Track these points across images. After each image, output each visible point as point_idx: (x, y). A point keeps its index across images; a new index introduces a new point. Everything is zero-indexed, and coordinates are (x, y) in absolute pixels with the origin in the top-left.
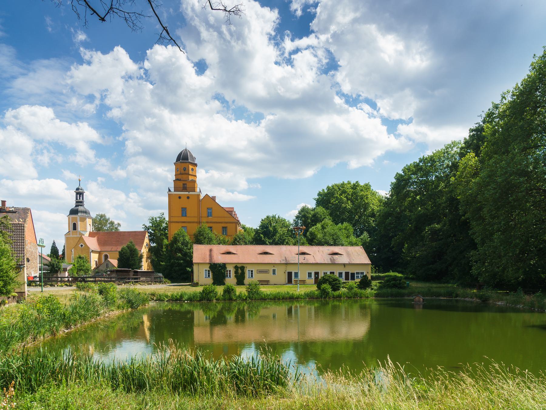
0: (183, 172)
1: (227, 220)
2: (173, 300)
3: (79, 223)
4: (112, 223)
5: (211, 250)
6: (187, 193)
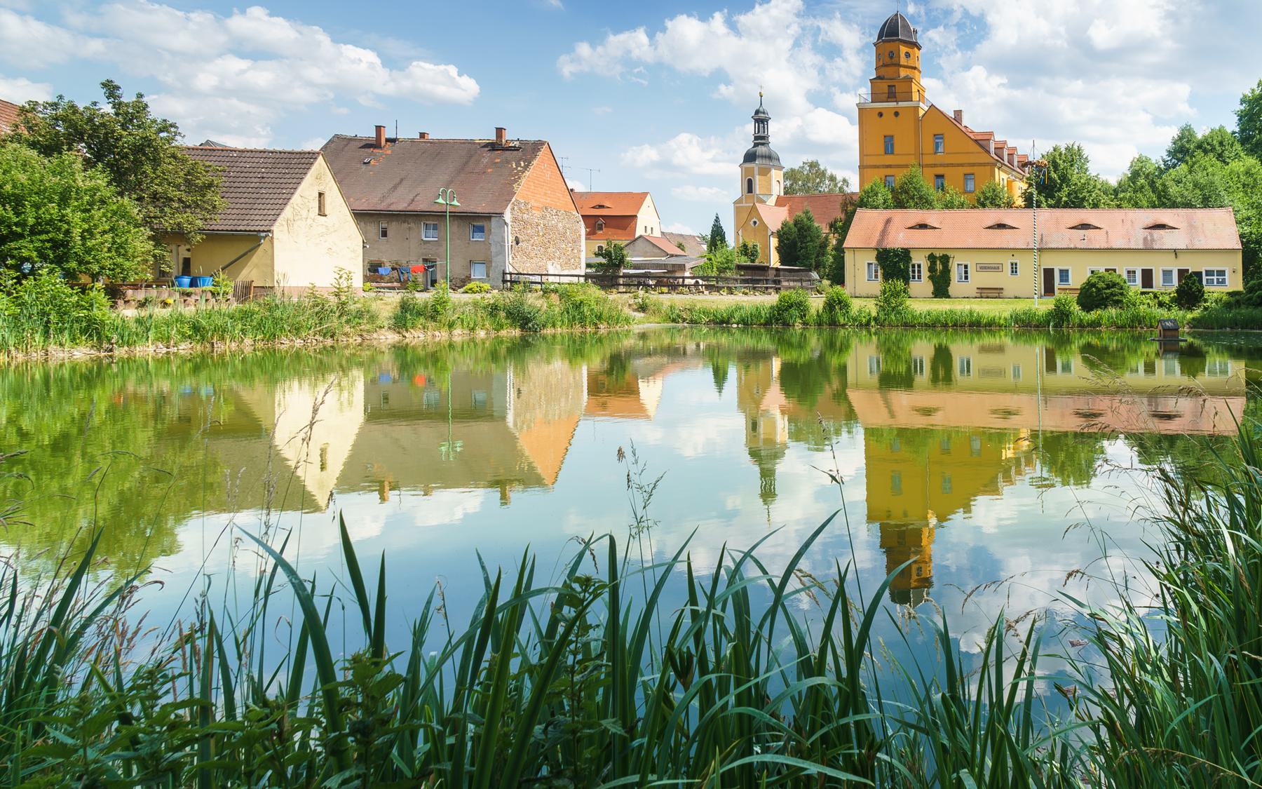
0: (887, 60)
2: (716, 323)
3: (757, 177)
4: (832, 179)
5: (888, 221)
6: (893, 104)
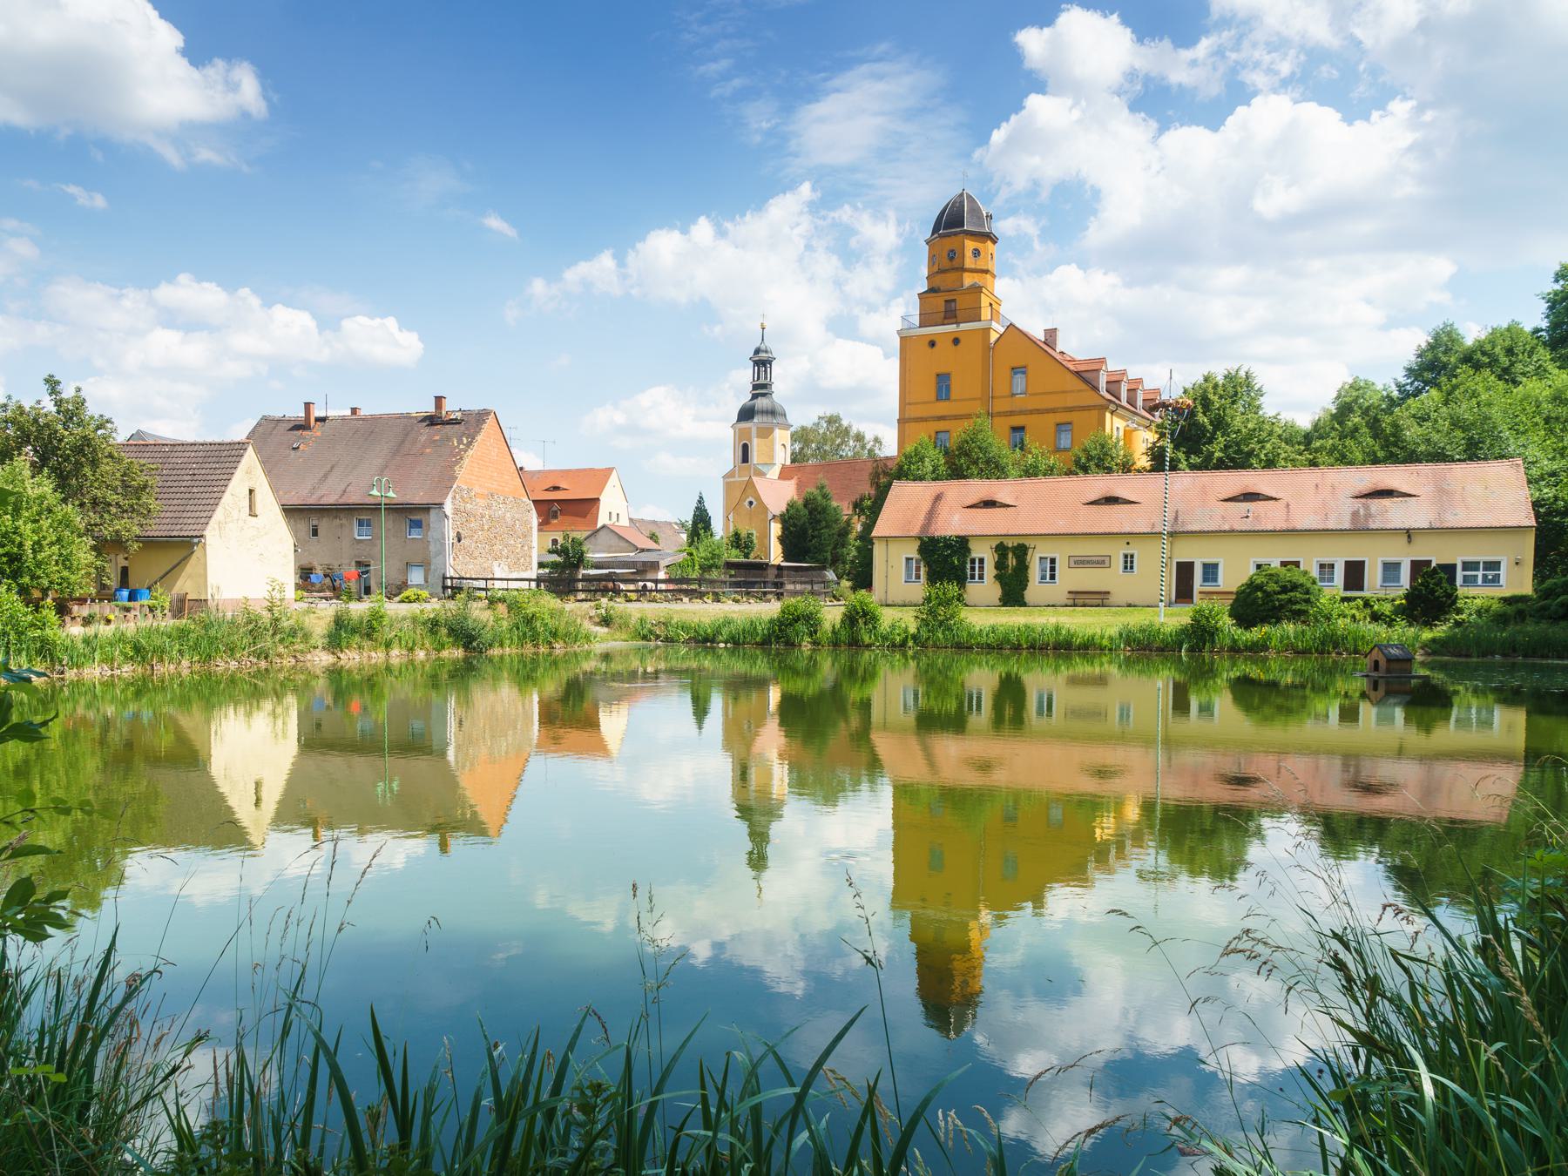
0: (946, 263)
1: (1070, 401)
4: (859, 438)
6: (952, 328)
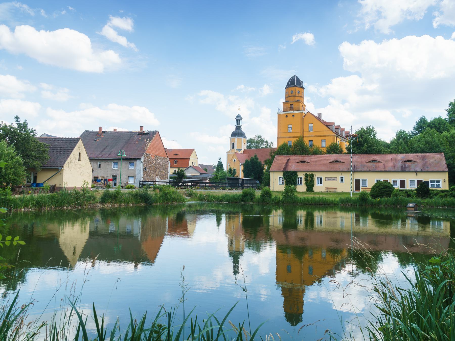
4: (267, 142)
